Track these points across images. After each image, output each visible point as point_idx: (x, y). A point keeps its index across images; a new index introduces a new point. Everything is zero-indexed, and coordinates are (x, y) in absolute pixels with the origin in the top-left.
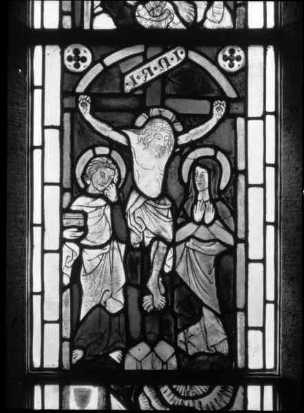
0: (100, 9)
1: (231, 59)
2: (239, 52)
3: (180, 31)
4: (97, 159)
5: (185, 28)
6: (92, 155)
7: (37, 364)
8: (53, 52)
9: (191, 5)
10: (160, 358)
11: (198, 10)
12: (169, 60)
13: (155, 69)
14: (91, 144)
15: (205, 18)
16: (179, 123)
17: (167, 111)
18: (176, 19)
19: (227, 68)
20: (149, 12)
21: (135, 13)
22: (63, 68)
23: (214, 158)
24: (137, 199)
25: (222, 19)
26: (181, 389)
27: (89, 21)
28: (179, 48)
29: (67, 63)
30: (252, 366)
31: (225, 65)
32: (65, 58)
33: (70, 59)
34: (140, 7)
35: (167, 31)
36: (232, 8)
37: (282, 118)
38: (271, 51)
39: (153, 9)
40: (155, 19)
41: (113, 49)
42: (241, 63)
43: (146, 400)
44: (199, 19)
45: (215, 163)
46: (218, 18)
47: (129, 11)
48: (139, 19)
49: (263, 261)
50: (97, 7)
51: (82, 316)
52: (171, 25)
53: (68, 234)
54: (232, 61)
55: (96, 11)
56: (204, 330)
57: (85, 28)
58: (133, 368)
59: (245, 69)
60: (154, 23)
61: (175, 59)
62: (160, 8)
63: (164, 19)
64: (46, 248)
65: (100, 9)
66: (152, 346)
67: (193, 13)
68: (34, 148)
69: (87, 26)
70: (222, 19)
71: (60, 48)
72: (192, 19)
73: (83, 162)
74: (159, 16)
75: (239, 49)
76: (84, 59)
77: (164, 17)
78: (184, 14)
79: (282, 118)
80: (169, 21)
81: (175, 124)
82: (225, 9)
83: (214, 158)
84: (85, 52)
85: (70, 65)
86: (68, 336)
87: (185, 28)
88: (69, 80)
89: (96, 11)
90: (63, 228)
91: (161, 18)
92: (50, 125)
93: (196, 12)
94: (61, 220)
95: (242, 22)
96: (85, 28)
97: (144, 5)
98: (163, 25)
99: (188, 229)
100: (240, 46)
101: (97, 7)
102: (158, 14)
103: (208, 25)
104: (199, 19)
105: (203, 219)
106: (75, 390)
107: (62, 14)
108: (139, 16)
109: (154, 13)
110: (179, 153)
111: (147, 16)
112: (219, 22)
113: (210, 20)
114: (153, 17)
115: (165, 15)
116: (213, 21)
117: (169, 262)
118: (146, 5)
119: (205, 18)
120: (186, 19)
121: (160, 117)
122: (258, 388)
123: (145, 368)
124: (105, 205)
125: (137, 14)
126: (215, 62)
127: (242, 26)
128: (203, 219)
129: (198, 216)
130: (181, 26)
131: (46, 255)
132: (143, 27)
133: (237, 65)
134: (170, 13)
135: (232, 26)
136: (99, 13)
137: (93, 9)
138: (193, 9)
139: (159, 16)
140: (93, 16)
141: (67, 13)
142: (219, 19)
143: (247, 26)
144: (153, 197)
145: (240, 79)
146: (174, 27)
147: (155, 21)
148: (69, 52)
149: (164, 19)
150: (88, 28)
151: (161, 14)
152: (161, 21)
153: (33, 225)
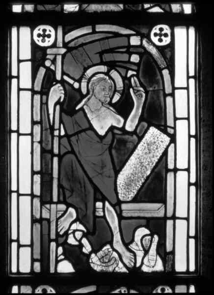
0: (62, 257)
1: (160, 35)
2: (166, 29)
3: (124, 273)
5: (128, 272)
7: (14, 270)
8: (25, 31)
9: (132, 254)
11: (137, 258)
15: (142, 263)
16: (120, 95)
18: (121, 265)
20: (99, 259)
21: (89, 260)
22: (33, 43)
25: (155, 265)
27: (54, 266)
28: (122, 288)
29: (36, 38)
34: (93, 255)
35: (114, 274)
36: (163, 256)
37: (201, 207)
38: (192, 31)
39: (103, 257)
40: (104, 265)
41: (71, 27)
44: (138, 265)
46: (152, 263)
47: (85, 258)
48: (92, 265)
50: (60, 255)
52: (117, 269)
55: (59, 259)
56: (138, 211)
57: (51, 272)
59: (172, 46)
60: (103, 268)
62: (108, 256)
63: (112, 265)
64: (21, 58)
65: (62, 257)
67: (134, 261)
68: (12, 241)
69: (52, 270)
70: (155, 265)
71: (32, 287)
72: (133, 264)
74: (108, 262)
75: (169, 288)
77: (111, 263)
78: (126, 261)
79: (201, 207)
80: (115, 266)
81: (117, 93)
82: (158, 257)
86: (39, 194)
87: (128, 272)
88: (38, 55)
89: (59, 259)
91: (109, 264)
93: (135, 259)
95: (170, 266)
96: (51, 272)
97: (96, 255)
98: (111, 269)
100: (168, 286)
101: (60, 255)
102: (107, 261)
103: (145, 269)
104: (138, 265)
107: (33, 260)
108: (92, 262)
109: (103, 260)
111: (99, 263)
112: (153, 267)
113: (146, 266)
114: (103, 263)
115: (112, 261)
116: (148, 266)
118: (98, 254)
119: (142, 263)
120: (128, 264)
125: (90, 261)
126: (150, 41)
127: (171, 270)
130: (124, 270)
131: (21, 92)
132: (95, 271)
133: (166, 41)
134: (116, 260)
135: (163, 270)
136: (61, 260)
137: (57, 257)
138: (133, 257)
139: (108, 262)
140: (57, 262)
142: (153, 265)
143: (175, 270)
145: (168, 52)
146: (119, 271)
147: (105, 266)
149: (112, 265)
150: (53, 272)
151: (109, 261)
152: (109, 266)
153: (11, 192)
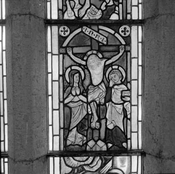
2: (128, 28)
4: (114, 70)
6: (70, 70)
10: (94, 145)
12: (89, 32)
13: (94, 35)
14: (120, 65)
17: (94, 51)
19: (123, 35)
23: (72, 70)
24: (102, 86)
26: (78, 158)
29: (60, 33)
30: (133, 148)
31: (123, 34)
32: (129, 31)
33: (128, 31)
42: (129, 33)
43: (84, 160)
45: (73, 71)
49: (53, 110)
51: (123, 130)
53: (128, 99)
54: (124, 31)
58: (99, 150)
59: (129, 36)
61: (87, 30)
66: (96, 142)
73: (123, 71)
76: (67, 31)
83: (72, 70)
84: (122, 28)
85: (62, 34)
88: (61, 39)
90: (130, 97)
92: (133, 57)
94: (131, 93)
99: (71, 98)
105: (76, 93)
106: (119, 158)
110: (106, 67)
117: (89, 110)
121: (92, 54)
122: (52, 158)
123: (103, 150)
124: (114, 88)
128: (76, 93)
129: (74, 93)
133: (128, 34)
141: (129, 13)
144: (94, 85)
145: (128, 40)
148: (61, 28)
